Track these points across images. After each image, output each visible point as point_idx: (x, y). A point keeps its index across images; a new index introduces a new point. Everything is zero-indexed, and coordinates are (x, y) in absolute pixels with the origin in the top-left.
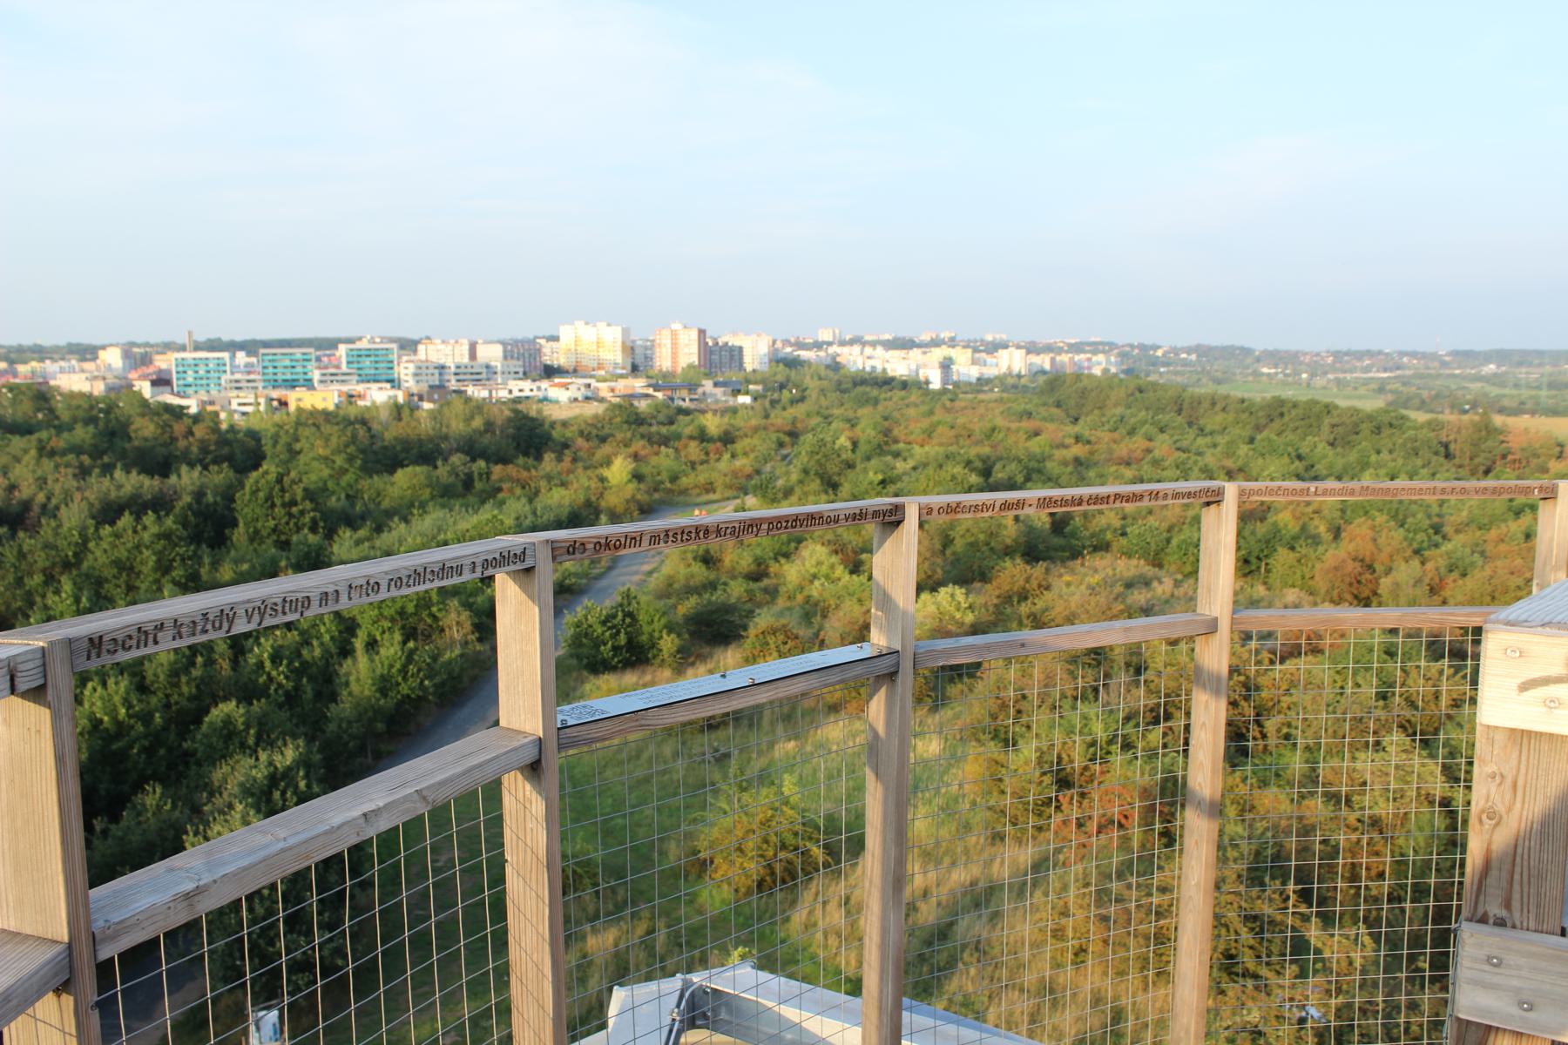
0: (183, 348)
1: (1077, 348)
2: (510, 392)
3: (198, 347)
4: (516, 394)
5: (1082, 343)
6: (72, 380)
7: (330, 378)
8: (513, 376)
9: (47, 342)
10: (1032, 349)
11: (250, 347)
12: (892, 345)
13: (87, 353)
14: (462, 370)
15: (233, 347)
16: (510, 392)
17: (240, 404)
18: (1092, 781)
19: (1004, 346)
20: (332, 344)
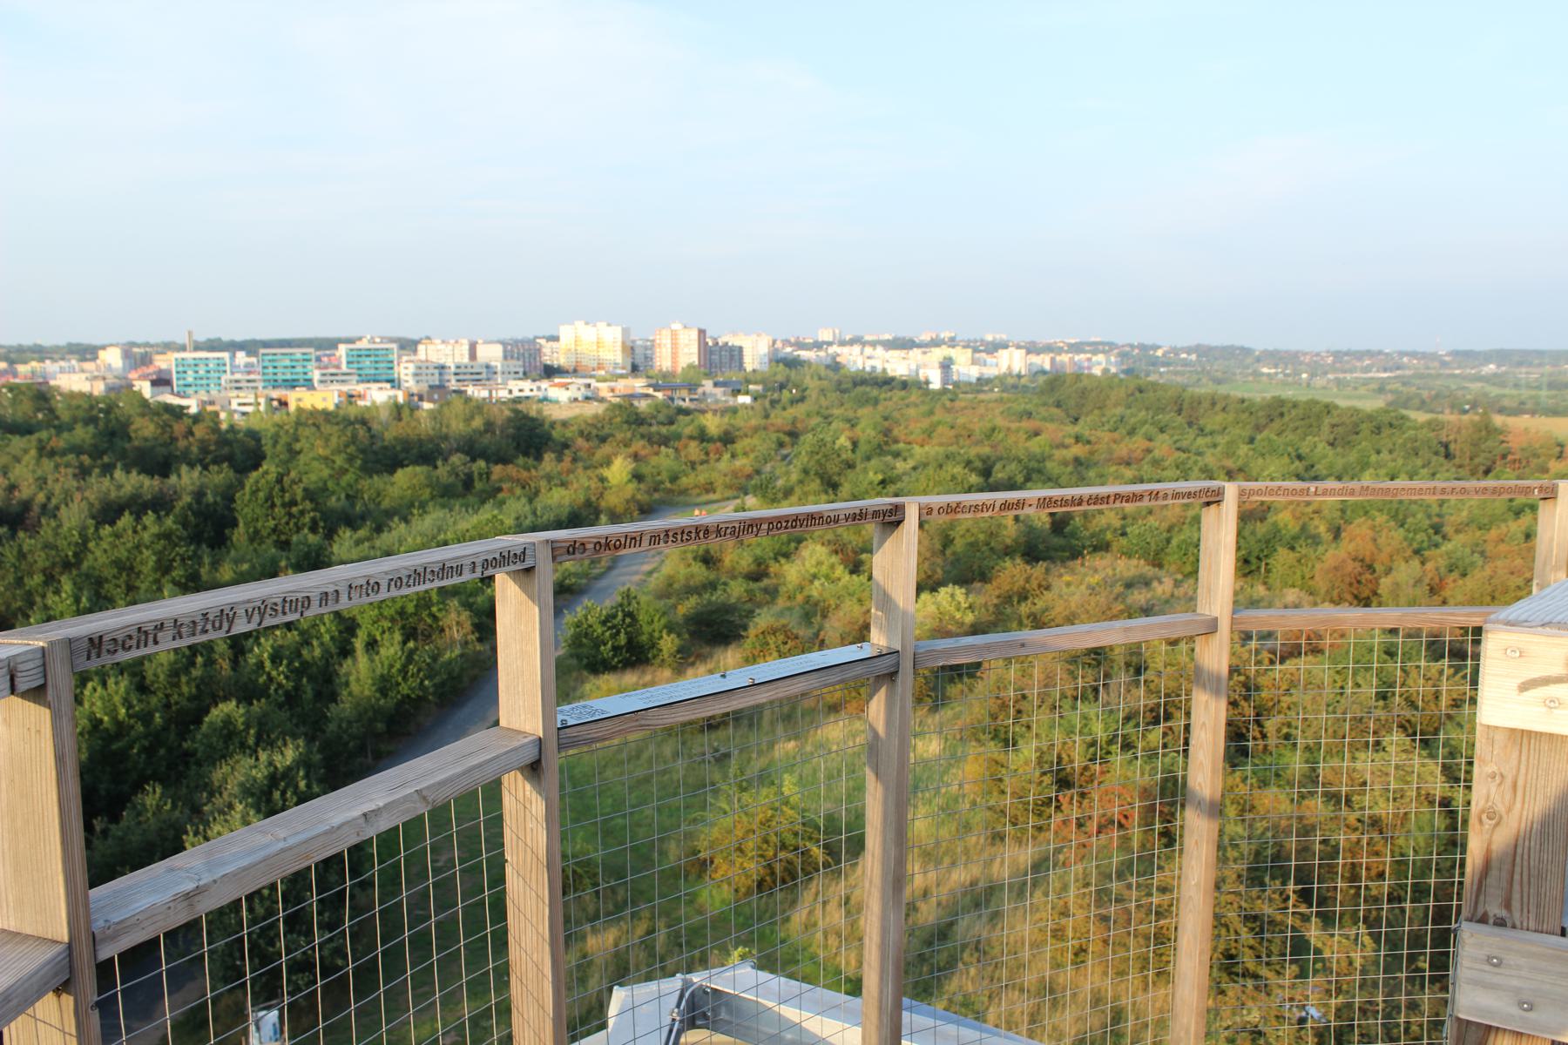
0: (183, 348)
1: (1077, 348)
2: (510, 392)
3: (198, 347)
4: (516, 394)
5: (1082, 343)
6: (72, 380)
7: (330, 378)
8: (513, 376)
9: (47, 342)
10: (1032, 349)
11: (250, 347)
12: (892, 345)
13: (87, 353)
14: (462, 370)
15: (233, 347)
16: (510, 392)
17: (240, 404)
18: (1092, 781)
19: (1004, 346)
20: (332, 344)
